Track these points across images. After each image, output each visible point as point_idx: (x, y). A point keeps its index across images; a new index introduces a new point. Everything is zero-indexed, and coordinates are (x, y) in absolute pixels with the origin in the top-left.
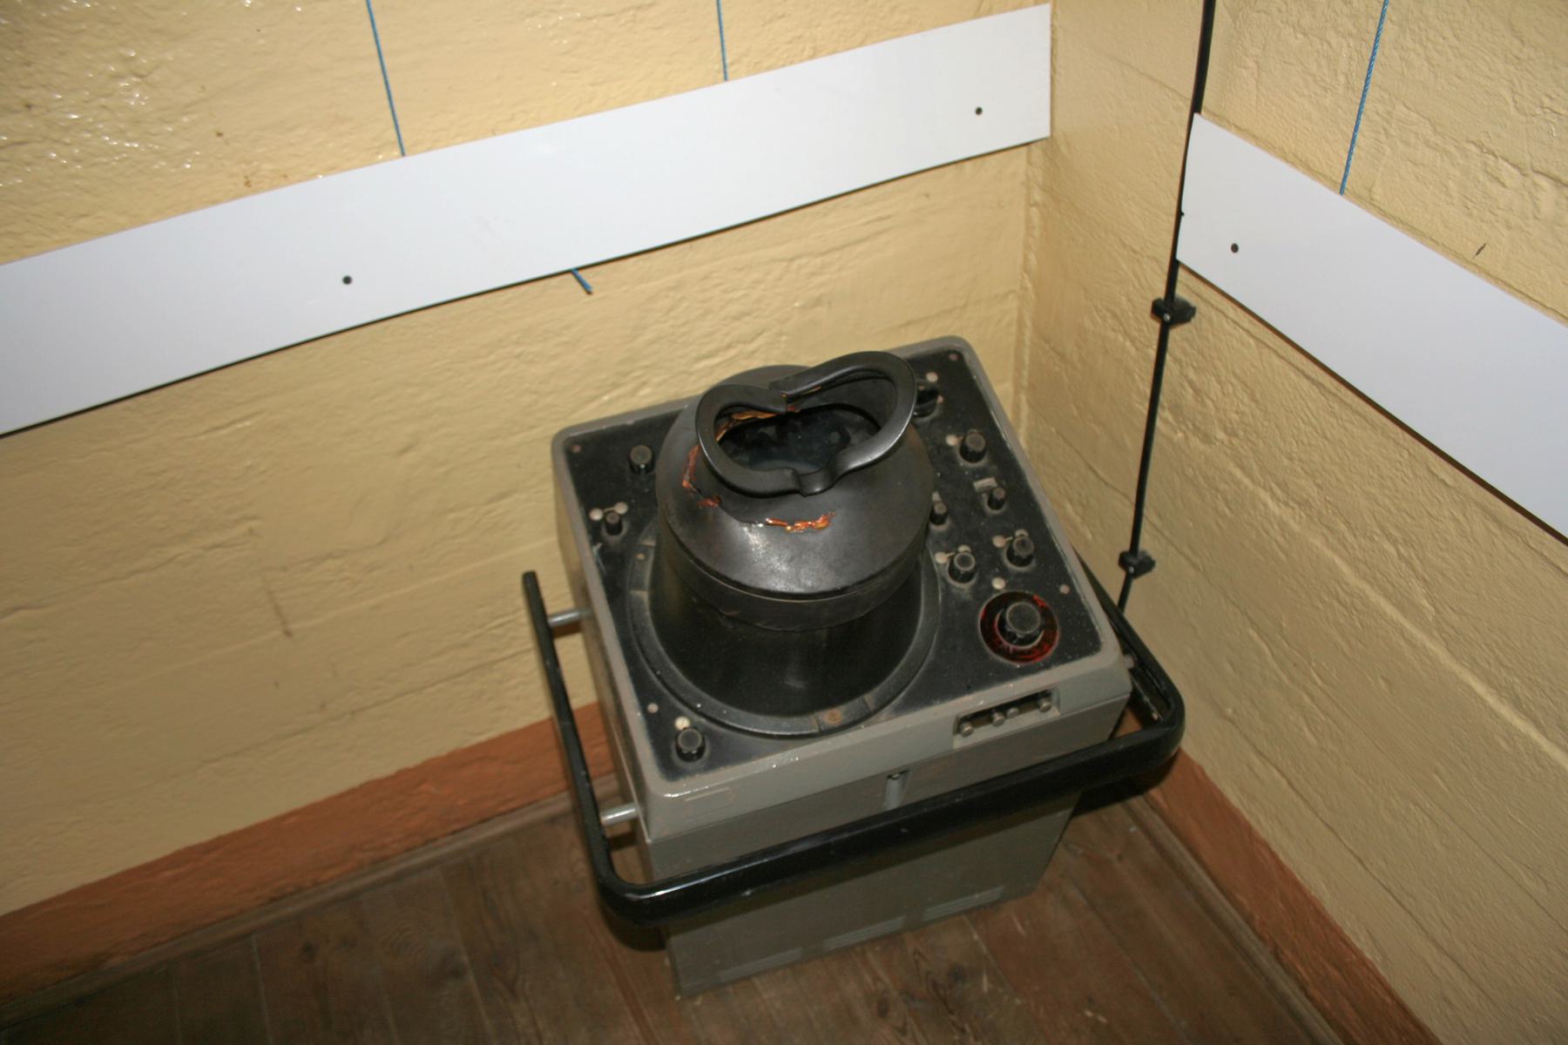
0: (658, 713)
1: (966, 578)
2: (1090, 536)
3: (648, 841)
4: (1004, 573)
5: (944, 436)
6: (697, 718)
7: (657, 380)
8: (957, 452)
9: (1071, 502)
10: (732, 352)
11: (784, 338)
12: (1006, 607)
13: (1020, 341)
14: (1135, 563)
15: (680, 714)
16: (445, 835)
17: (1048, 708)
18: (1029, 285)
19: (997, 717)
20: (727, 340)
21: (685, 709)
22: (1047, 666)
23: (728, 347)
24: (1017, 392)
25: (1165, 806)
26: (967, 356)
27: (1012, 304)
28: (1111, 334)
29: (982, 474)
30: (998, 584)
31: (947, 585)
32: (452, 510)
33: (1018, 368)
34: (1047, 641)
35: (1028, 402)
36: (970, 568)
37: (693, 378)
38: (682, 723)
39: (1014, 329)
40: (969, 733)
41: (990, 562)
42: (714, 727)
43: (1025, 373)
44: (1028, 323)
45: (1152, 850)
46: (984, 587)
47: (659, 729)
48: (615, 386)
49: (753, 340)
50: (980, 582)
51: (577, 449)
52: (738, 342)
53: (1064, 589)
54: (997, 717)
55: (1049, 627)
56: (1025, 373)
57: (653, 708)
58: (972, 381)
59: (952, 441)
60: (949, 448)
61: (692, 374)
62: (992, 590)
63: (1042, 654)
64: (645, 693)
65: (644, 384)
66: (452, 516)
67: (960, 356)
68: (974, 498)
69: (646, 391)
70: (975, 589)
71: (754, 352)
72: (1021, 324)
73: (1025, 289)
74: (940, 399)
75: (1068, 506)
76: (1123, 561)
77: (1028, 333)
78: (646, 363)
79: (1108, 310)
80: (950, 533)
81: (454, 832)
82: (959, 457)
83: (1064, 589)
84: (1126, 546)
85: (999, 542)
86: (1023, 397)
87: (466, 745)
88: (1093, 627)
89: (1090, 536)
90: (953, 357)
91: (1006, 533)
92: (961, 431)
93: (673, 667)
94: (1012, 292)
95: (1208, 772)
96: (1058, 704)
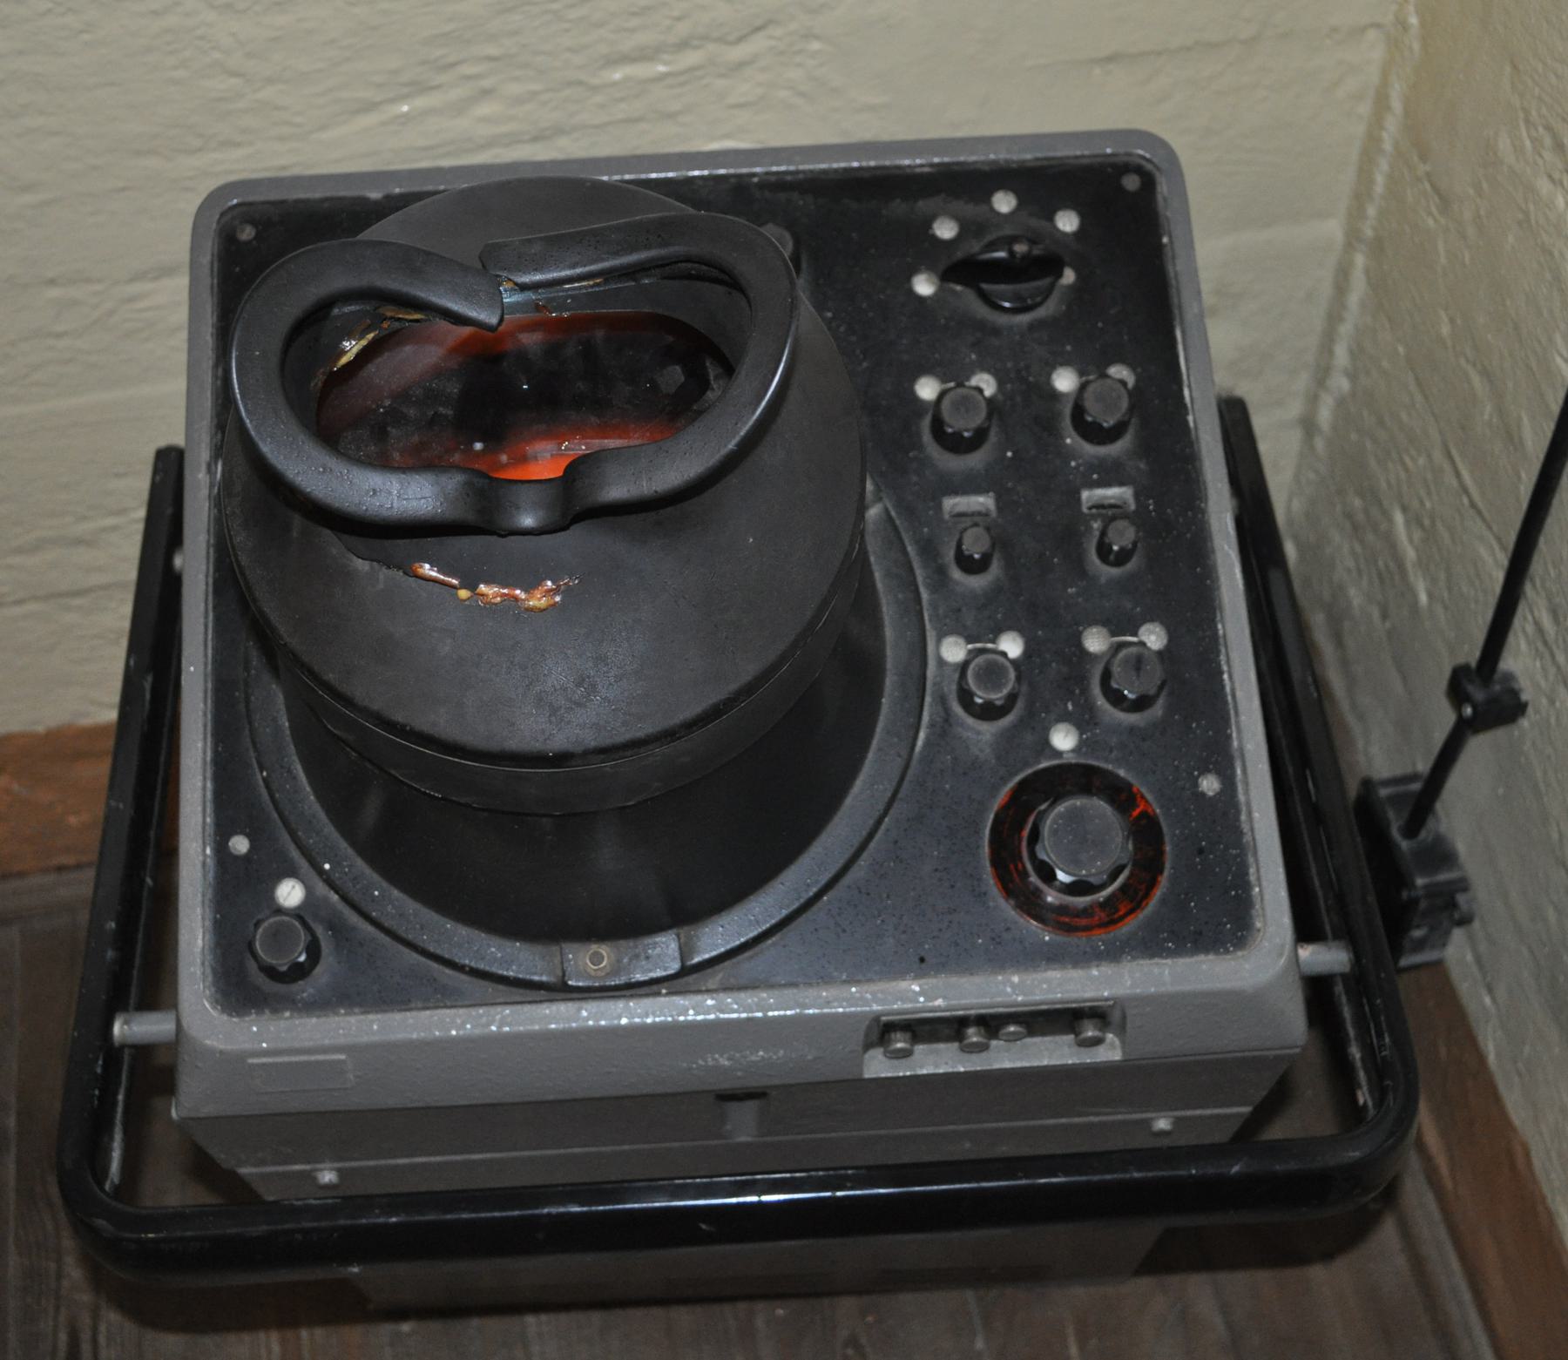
0: (246, 858)
1: (989, 712)
2: (1423, 598)
3: (174, 1114)
4: (1084, 720)
5: (1051, 367)
6: (322, 889)
7: (516, 89)
8: (1067, 411)
9: (1405, 509)
10: (691, 58)
11: (815, 46)
12: (1057, 799)
13: (1372, 144)
14: (1484, 697)
15: (292, 873)
16: (45, 871)
17: (1097, 1042)
18: (1414, 20)
19: (973, 1035)
20: (683, 29)
21: (303, 864)
22: (1113, 954)
23: (683, 45)
24: (1349, 246)
25: (1449, 1184)
26: (1163, 188)
27: (1373, 51)
28: (1544, 186)
29: (1110, 474)
30: (1063, 740)
31: (948, 717)
32: (52, 282)
33: (1361, 195)
34: (1134, 896)
35: (1367, 271)
36: (998, 697)
37: (599, 99)
38: (290, 893)
39: (1365, 108)
40: (906, 1054)
41: (1057, 678)
42: (353, 918)
43: (1371, 211)
44: (1397, 105)
45: (1401, 1261)
46: (1029, 738)
47: (240, 887)
48: (419, 88)
49: (740, 39)
50: (1021, 724)
51: (247, 233)
52: (706, 38)
53: (1209, 785)
54: (973, 1035)
55: (1147, 865)
56: (1371, 211)
57: (240, 845)
58: (1158, 250)
59: (1065, 381)
60: (1055, 396)
61: (595, 89)
62: (1045, 747)
63: (1112, 922)
64: (231, 808)
65: (486, 93)
66: (54, 292)
67: (1149, 182)
68: (1068, 536)
69: (486, 109)
70: (1007, 740)
71: (740, 65)
72: (1381, 103)
73: (1403, 25)
74: (1069, 276)
75: (1399, 518)
76: (1457, 689)
77: (1392, 124)
78: (493, 51)
79: (1548, 128)
80: (992, 596)
81: (60, 869)
82: (1067, 422)
83: (1209, 785)
84: (1471, 653)
85: (1095, 642)
86: (1360, 260)
87: (86, 722)
88: (1246, 886)
89: (1423, 598)
90: (1131, 183)
91: (1122, 624)
92: (1092, 365)
93: (299, 770)
94: (1378, 26)
95: (1537, 1163)
96: (1121, 1031)
